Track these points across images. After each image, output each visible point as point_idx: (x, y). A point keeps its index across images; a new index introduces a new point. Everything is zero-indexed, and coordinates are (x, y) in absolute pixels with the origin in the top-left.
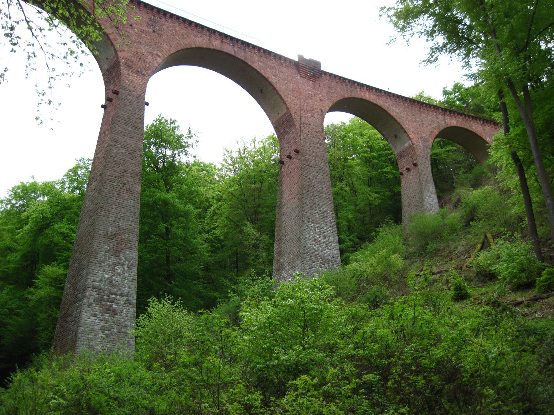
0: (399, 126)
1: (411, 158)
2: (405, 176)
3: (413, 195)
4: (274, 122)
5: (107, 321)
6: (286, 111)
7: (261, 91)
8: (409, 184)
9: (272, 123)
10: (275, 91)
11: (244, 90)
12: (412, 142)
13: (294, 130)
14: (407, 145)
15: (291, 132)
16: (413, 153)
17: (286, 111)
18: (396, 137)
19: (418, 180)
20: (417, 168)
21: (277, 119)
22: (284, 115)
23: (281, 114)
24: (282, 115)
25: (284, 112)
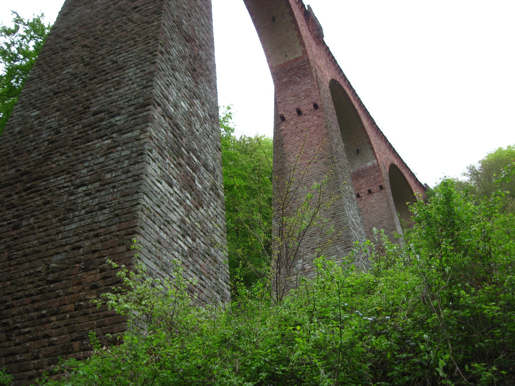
0: (367, 140)
1: (374, 179)
2: (363, 198)
3: (378, 220)
4: (274, 66)
5: (169, 223)
6: (301, 54)
7: (274, 20)
8: (370, 208)
9: (271, 67)
10: (294, 25)
11: (247, 10)
12: (378, 161)
13: (309, 81)
14: (369, 164)
15: (303, 83)
16: (377, 174)
17: (301, 54)
18: (358, 152)
19: (386, 204)
20: (383, 191)
21: (282, 62)
22: (296, 60)
23: (291, 58)
24: (291, 59)
25: (297, 56)
